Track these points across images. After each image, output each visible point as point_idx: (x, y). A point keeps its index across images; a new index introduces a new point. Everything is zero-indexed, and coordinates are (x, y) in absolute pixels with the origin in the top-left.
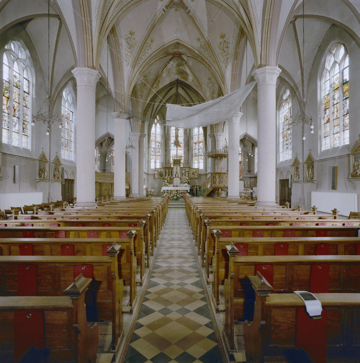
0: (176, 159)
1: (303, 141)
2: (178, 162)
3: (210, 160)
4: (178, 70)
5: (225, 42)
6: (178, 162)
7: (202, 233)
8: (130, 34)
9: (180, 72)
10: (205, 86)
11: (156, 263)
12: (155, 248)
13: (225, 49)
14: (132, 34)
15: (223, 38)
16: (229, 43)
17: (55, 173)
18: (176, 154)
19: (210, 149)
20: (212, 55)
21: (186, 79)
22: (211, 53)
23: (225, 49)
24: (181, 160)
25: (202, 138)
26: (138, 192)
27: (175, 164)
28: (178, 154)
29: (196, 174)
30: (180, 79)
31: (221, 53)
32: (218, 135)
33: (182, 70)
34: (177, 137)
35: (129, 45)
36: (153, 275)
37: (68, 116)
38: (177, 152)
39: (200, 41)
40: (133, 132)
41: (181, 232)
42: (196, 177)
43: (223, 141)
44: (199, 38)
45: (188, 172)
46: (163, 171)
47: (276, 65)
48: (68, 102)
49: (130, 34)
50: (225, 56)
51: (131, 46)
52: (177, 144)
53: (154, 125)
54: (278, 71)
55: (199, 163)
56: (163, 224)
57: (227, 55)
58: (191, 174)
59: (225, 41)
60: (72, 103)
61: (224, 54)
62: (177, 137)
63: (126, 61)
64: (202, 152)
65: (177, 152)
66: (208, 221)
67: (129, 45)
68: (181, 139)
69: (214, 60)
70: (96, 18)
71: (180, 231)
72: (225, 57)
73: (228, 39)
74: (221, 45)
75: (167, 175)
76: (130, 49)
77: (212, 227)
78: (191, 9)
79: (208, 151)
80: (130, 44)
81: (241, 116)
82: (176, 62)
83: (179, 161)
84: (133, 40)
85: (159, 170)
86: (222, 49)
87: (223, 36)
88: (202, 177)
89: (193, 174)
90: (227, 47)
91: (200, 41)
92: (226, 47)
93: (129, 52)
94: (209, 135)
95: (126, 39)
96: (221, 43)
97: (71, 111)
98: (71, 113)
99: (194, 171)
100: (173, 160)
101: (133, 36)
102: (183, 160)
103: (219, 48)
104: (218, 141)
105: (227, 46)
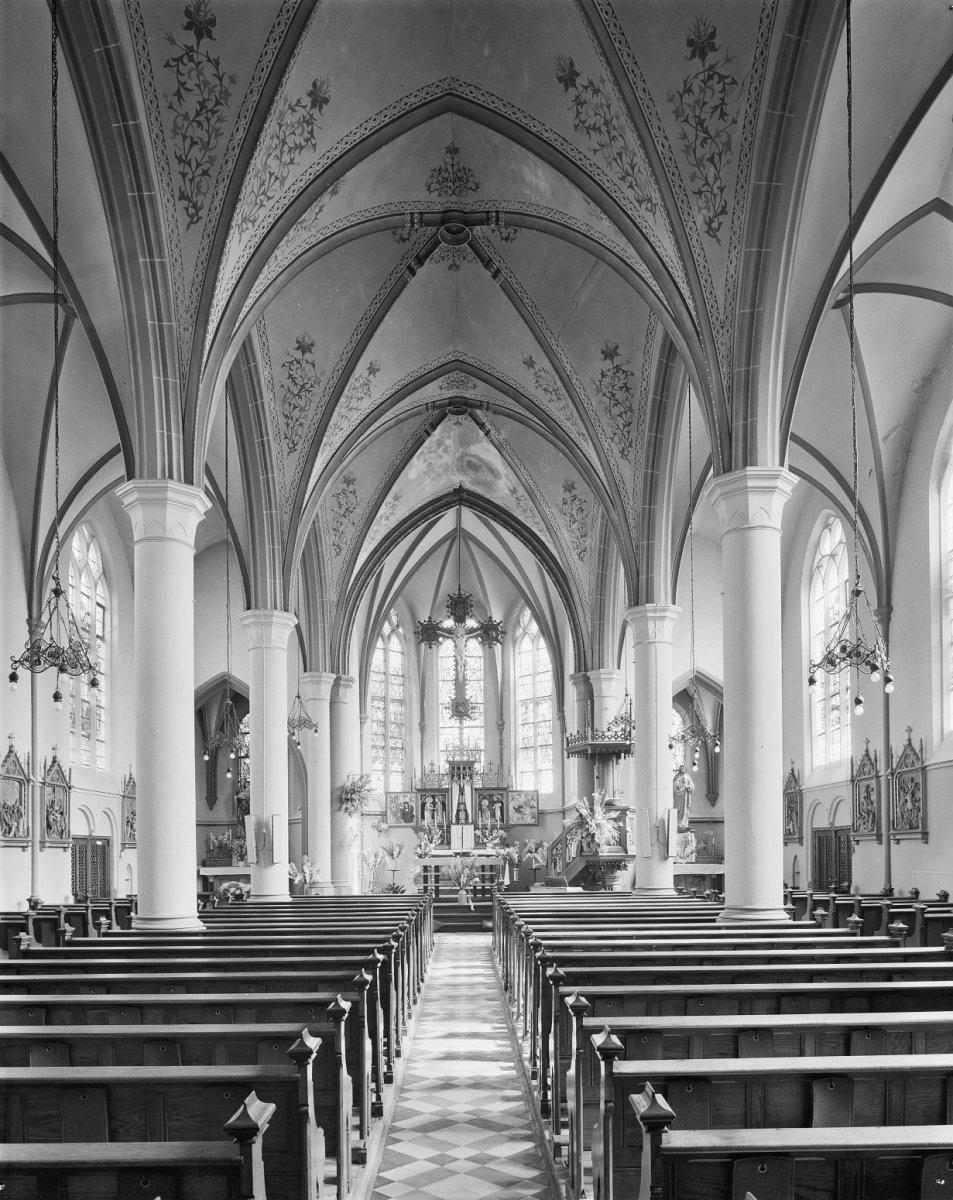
0: (457, 759)
1: (887, 696)
2: (464, 768)
3: (574, 764)
4: (461, 458)
5: (710, 77)
6: (467, 770)
7: (540, 1009)
8: (298, 348)
9: (469, 462)
10: (555, 511)
11: (402, 1104)
12: (396, 1059)
14: (304, 347)
16: (632, 374)
17: (51, 817)
18: (457, 743)
19: (573, 728)
20: (575, 413)
21: (488, 485)
22: (571, 406)
23: (713, 124)
24: (473, 762)
25: (547, 686)
26: (329, 880)
27: (456, 778)
28: (466, 743)
29: (527, 811)
30: (468, 486)
31: (606, 408)
32: (649, 614)
33: (476, 457)
34: (460, 685)
35: (296, 384)
36: (393, 1135)
37: (88, 620)
38: (461, 734)
39: (533, 367)
40: (311, 670)
41: (476, 1009)
42: (529, 820)
43: (616, 691)
44: (531, 358)
45: (502, 803)
46: (414, 803)
48: (89, 572)
49: (298, 348)
50: (620, 415)
51: (303, 387)
52: (460, 709)
53: (380, 644)
54: (790, 482)
55: (537, 772)
56: (418, 984)
57: (720, 154)
58: (511, 811)
59: (575, 497)
60: (103, 577)
61: (616, 411)
62: (460, 685)
63: (286, 438)
64: (547, 733)
65: (461, 734)
66: (556, 971)
67: (296, 384)
68: (475, 692)
69: (584, 431)
70: (194, 317)
71: (475, 1007)
72: (621, 422)
73: (728, 60)
74: (606, 381)
75: (427, 814)
76: (300, 397)
77: (563, 989)
79: (568, 735)
80: (300, 381)
82: (456, 431)
83: (469, 765)
85: (402, 799)
86: (693, 121)
88: (549, 819)
89: (518, 810)
90: (626, 388)
91: (533, 367)
92: (621, 388)
94: (572, 677)
95: (284, 365)
96: (603, 375)
97: (98, 604)
98: (100, 610)
99: (522, 799)
100: (449, 762)
101: (308, 355)
102: (483, 763)
103: (599, 390)
104: (601, 697)
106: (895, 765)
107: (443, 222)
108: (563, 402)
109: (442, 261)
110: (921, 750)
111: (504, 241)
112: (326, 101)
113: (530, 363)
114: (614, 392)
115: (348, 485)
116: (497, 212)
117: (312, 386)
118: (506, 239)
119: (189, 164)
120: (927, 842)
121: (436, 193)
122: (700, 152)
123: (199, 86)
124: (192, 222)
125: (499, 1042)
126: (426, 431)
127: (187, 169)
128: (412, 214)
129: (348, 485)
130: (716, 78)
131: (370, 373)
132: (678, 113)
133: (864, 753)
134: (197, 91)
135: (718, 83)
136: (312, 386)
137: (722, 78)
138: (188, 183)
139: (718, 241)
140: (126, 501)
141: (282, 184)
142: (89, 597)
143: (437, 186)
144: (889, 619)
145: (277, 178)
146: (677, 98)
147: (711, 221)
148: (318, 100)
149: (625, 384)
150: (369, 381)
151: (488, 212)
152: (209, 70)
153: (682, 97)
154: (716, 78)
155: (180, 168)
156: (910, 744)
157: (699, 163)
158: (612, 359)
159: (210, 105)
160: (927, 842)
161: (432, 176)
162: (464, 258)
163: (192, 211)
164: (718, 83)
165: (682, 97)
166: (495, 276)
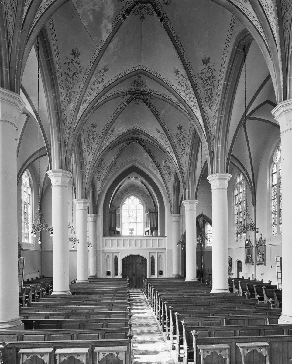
5: (209, 70)
13: (168, 170)
15: (180, 129)
16: (215, 70)
47: (227, 172)
50: (209, 89)
63: (87, 151)
72: (209, 92)
78: (165, 16)
81: (197, 203)
84: (76, 65)
87: (180, 128)
93: (71, 83)
101: (95, 129)
105: (212, 75)
106: (257, 244)
107: (135, 94)
108: (167, 143)
109: (138, 15)
110: (264, 240)
111: (165, 4)
112: (108, 70)
113: (159, 131)
114: (207, 79)
115: (93, 128)
116: (151, 93)
117: (78, 74)
118: (152, 98)
119: (69, 88)
120: (266, 266)
121: (134, 86)
122: (206, 88)
123: (74, 69)
124: (69, 103)
125: (133, 311)
126: (125, 104)
127: (69, 89)
128: (126, 139)
129: (93, 128)
130: (210, 69)
131: (104, 71)
132: (176, 138)
133: (260, 238)
134: (73, 70)
135: (211, 71)
136: (78, 74)
137: (212, 69)
138: (68, 93)
139: (212, 110)
140: (75, 202)
141: (94, 91)
142: (26, 192)
143: (134, 84)
144: (255, 205)
145: (93, 90)
146: (176, 136)
147: (210, 105)
148: (105, 70)
149: (212, 75)
150: (103, 75)
151: (148, 92)
152: (94, 132)
153: (177, 135)
154: (210, 69)
155: (67, 89)
156: (261, 239)
157: (180, 145)
158: (207, 64)
159: (76, 74)
160: (266, 266)
161: (133, 82)
162: (148, 14)
163: (89, 153)
164: (211, 71)
165: (177, 135)
166: (161, 20)
